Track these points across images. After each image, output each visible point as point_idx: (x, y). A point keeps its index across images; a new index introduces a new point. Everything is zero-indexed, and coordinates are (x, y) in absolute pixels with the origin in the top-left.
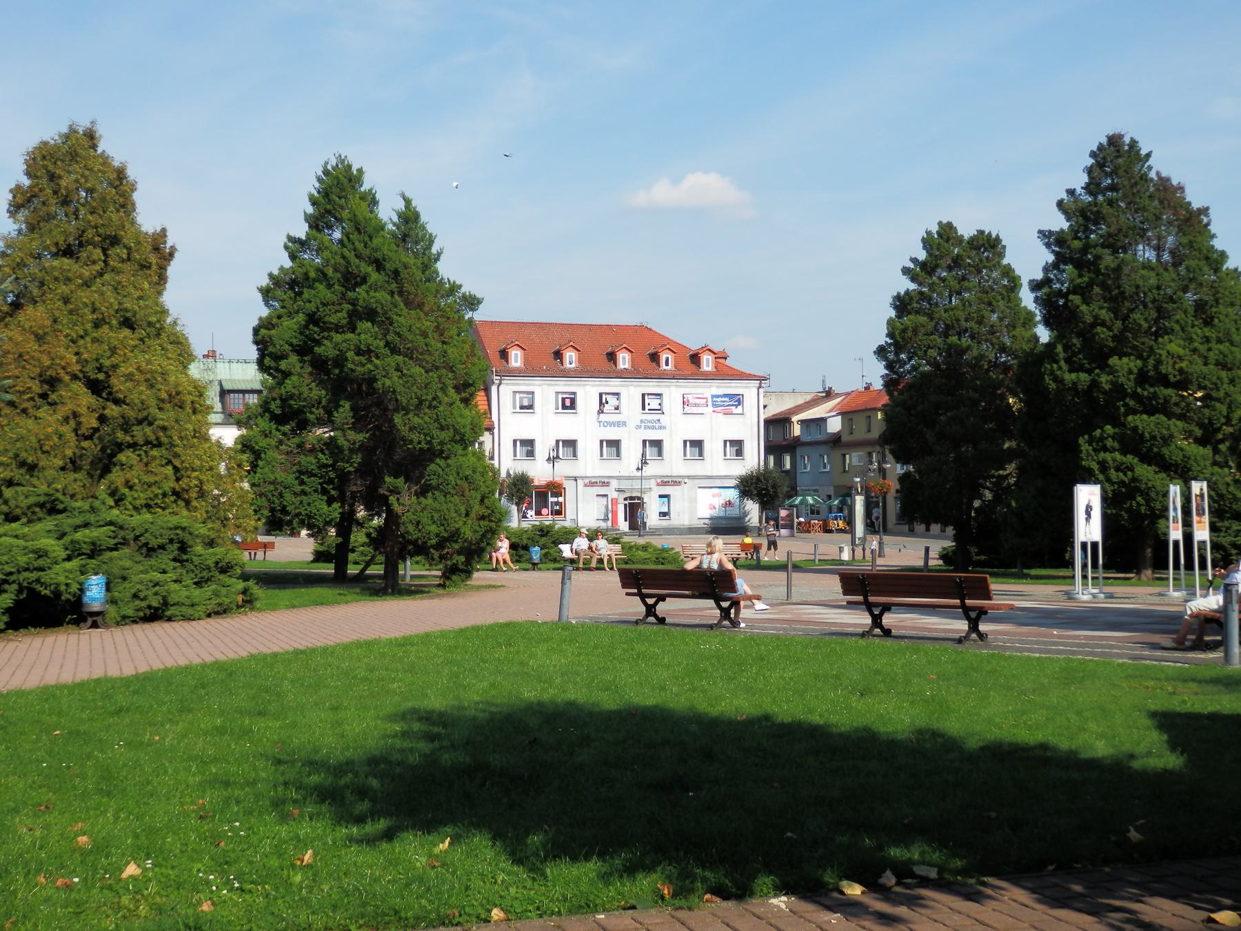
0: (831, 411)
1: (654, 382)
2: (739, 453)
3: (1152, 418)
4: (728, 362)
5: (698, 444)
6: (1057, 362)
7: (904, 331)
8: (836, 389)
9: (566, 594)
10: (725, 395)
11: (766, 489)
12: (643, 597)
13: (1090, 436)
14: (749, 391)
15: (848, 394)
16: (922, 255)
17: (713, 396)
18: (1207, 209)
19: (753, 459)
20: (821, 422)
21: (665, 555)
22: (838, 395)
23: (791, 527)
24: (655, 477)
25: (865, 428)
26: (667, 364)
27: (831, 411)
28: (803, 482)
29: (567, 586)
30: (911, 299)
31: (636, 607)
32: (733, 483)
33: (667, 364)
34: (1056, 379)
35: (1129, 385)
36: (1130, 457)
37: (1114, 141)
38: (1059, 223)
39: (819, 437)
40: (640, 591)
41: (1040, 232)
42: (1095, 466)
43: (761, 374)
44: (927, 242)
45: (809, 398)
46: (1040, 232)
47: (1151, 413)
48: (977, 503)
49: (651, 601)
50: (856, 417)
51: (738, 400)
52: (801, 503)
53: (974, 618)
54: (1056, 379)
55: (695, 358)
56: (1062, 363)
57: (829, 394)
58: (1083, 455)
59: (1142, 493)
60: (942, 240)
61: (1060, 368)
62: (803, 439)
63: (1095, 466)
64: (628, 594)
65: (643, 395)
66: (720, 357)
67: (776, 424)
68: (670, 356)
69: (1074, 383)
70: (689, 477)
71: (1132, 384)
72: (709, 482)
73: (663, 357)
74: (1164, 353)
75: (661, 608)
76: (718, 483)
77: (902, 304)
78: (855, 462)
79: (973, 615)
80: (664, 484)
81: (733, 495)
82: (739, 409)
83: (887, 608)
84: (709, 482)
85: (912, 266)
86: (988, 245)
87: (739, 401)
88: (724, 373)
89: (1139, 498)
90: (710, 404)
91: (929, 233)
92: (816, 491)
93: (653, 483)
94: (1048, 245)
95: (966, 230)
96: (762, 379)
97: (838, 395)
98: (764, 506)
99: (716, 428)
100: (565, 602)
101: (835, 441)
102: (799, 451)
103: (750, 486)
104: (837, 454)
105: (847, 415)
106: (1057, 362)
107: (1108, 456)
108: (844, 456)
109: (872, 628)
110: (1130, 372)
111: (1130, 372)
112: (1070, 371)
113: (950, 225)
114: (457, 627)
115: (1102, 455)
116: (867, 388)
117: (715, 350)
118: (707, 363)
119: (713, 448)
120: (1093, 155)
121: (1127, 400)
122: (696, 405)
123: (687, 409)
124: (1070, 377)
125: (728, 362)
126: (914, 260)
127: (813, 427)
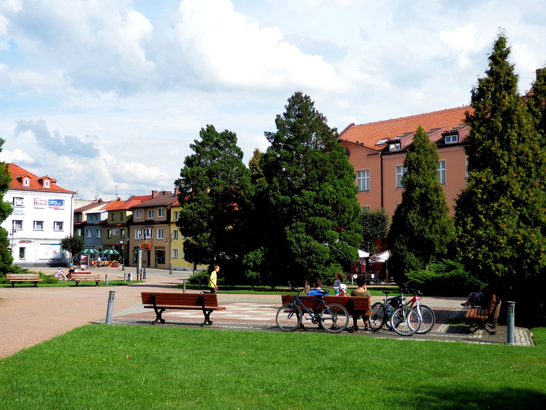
0: (101, 210)
1: (20, 192)
2: (61, 228)
3: (321, 219)
4: (57, 184)
5: (40, 223)
6: (276, 191)
7: (192, 173)
8: (104, 200)
9: (111, 308)
10: (55, 200)
11: (76, 246)
12: (156, 308)
13: (290, 226)
14: (67, 198)
15: (109, 202)
16: (200, 140)
17: (49, 200)
18: (337, 129)
19: (68, 232)
20: (97, 215)
21: (52, 278)
22: (104, 203)
23: (87, 264)
24: (18, 239)
25: (119, 218)
26: (26, 183)
27: (101, 210)
28: (87, 242)
29: (111, 304)
30: (195, 158)
31: (150, 314)
32: (59, 242)
33: (26, 183)
34: (275, 198)
35: (311, 203)
36: (309, 236)
37: (298, 95)
38: (274, 130)
39: (96, 222)
40: (155, 305)
41: (265, 132)
42: (294, 240)
43: (74, 191)
44: (202, 133)
45: (89, 203)
46: (265, 132)
47: (321, 216)
48: (228, 258)
49: (159, 310)
50: (115, 213)
51: (61, 202)
52: (87, 252)
53: (207, 313)
54: (275, 198)
55: (41, 181)
56: (278, 191)
57: (100, 202)
58: (288, 235)
59: (314, 253)
60: (209, 133)
61: (278, 194)
62: (88, 222)
63: (294, 240)
64: (145, 307)
65: (14, 198)
66: (53, 182)
67: (78, 214)
68: (28, 180)
69: (284, 200)
70: (36, 239)
71: (312, 202)
72: (45, 242)
73: (25, 180)
74: (326, 190)
75: (164, 315)
76: (50, 242)
77: (189, 162)
78: (114, 233)
79: (159, 310)
80: (23, 242)
81: (58, 248)
82: (62, 207)
83: (163, 309)
84: (45, 242)
85: (195, 144)
86: (230, 137)
87: (62, 203)
88: (55, 190)
89: (313, 255)
90: (48, 204)
91: (203, 129)
92: (94, 247)
93: (17, 242)
94: (268, 138)
95: (219, 130)
96: (74, 193)
97: (104, 203)
98: (73, 254)
99: (49, 216)
100: (110, 312)
101: (104, 224)
102: (86, 228)
103: (66, 244)
104: (105, 230)
105: (111, 212)
106: (276, 191)
107: (300, 236)
108: (108, 231)
109: (157, 320)
110: (311, 197)
111: (311, 197)
112: (282, 195)
113: (212, 126)
114: (70, 329)
115: (297, 235)
116: (119, 200)
117: (51, 178)
118: (47, 184)
119: (48, 225)
120: (289, 100)
121: (309, 209)
122: (41, 204)
123: (36, 206)
124: (282, 198)
125: (57, 184)
126: (196, 141)
127: (93, 217)
